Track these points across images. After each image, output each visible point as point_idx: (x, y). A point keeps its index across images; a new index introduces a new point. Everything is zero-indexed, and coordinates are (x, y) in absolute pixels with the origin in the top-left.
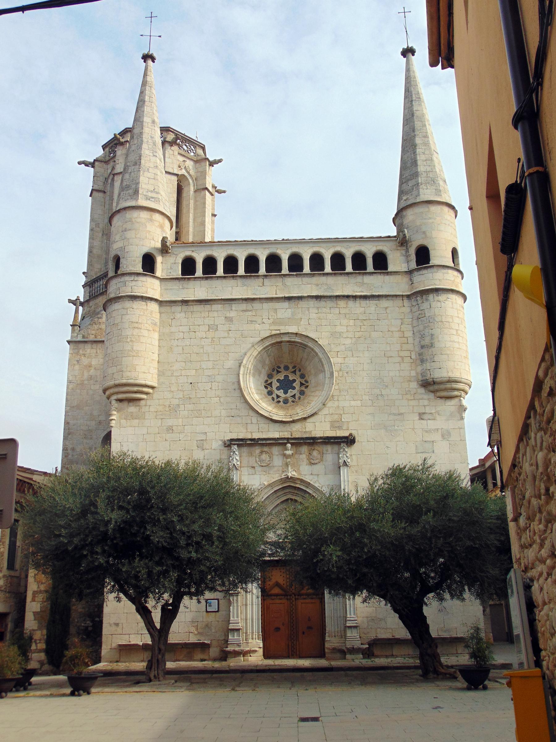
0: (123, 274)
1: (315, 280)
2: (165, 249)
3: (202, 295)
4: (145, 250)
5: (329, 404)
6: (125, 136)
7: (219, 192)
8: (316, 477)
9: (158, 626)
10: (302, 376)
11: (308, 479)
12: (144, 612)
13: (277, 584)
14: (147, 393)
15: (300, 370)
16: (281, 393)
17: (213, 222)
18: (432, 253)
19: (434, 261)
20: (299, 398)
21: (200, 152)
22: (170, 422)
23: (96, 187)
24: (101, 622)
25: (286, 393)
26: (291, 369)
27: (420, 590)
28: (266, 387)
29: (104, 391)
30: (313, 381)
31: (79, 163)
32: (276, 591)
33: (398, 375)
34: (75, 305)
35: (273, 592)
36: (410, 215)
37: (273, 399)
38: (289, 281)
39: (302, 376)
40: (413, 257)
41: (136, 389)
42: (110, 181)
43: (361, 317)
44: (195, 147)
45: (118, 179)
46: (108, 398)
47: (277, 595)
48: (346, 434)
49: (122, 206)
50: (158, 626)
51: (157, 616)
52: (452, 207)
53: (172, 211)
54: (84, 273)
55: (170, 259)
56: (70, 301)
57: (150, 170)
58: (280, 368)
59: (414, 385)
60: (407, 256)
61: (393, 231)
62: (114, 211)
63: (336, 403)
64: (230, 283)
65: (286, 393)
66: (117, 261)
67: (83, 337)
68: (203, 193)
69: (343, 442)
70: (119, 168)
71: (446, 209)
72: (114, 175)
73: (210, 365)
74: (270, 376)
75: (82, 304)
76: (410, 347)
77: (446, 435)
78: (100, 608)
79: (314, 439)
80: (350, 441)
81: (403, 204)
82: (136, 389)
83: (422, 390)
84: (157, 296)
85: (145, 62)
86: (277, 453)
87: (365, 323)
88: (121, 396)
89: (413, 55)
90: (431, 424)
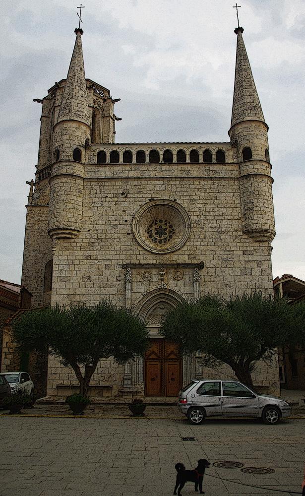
0: (61, 161)
1: (179, 167)
2: (87, 146)
3: (109, 175)
4: (75, 147)
5: (188, 244)
6: (62, 84)
7: (117, 119)
8: (179, 288)
9: (83, 376)
10: (171, 226)
11: (174, 289)
12: (77, 369)
13: (153, 352)
14: (75, 235)
15: (169, 223)
16: (157, 237)
17: (113, 137)
18: (254, 153)
19: (255, 157)
20: (169, 240)
21: (106, 94)
22: (89, 253)
23: (44, 115)
24: (46, 372)
25: (160, 237)
26: (164, 222)
27: (252, 360)
28: (148, 233)
29: (49, 232)
30: (177, 230)
31: (35, 100)
32: (153, 356)
33: (230, 227)
34: (30, 185)
35: (151, 357)
36: (239, 129)
37: (152, 240)
38: (164, 168)
39: (171, 226)
40: (241, 155)
41: (68, 232)
42: (52, 111)
43: (208, 191)
44: (103, 91)
45: (57, 109)
46: (51, 237)
47: (153, 359)
48: (199, 262)
49: (60, 120)
50: (83, 376)
51: (83, 370)
52: (266, 125)
53: (90, 122)
54: (36, 166)
55: (90, 154)
56: (28, 183)
57: (79, 98)
58: (156, 221)
59: (240, 233)
60: (237, 153)
61: (228, 140)
62: (56, 123)
63: (192, 243)
64: (128, 168)
65: (160, 237)
66: (58, 153)
67: (35, 203)
68: (108, 119)
69: (196, 267)
70: (57, 103)
71: (262, 125)
72: (55, 107)
73: (114, 218)
74: (151, 226)
75: (34, 184)
76: (238, 210)
77: (259, 264)
78: (46, 362)
79: (178, 264)
80: (201, 266)
81: (235, 122)
82: (68, 232)
83: (245, 236)
84: (82, 175)
85: (76, 34)
86: (154, 273)
87: (210, 194)
88: (58, 236)
89: (242, 32)
90: (250, 258)
